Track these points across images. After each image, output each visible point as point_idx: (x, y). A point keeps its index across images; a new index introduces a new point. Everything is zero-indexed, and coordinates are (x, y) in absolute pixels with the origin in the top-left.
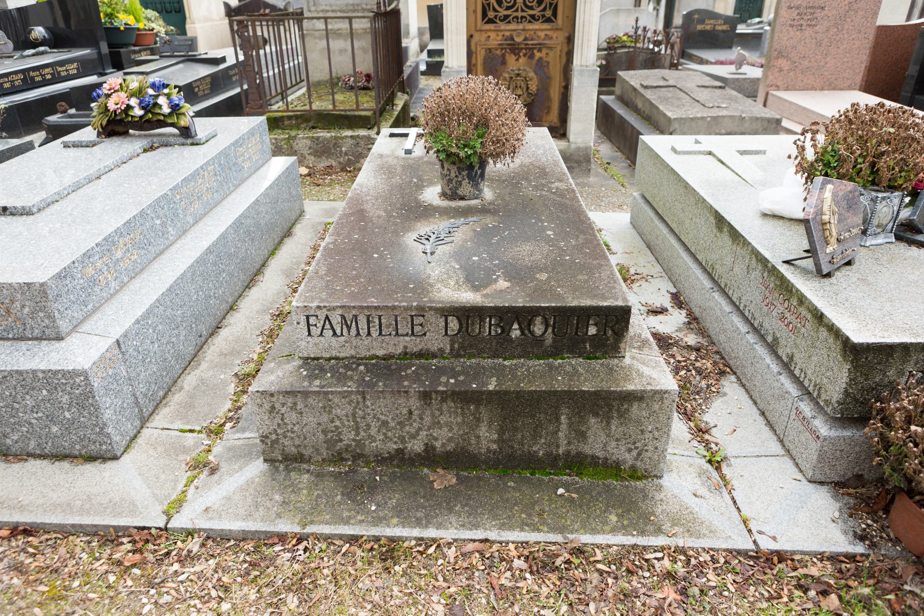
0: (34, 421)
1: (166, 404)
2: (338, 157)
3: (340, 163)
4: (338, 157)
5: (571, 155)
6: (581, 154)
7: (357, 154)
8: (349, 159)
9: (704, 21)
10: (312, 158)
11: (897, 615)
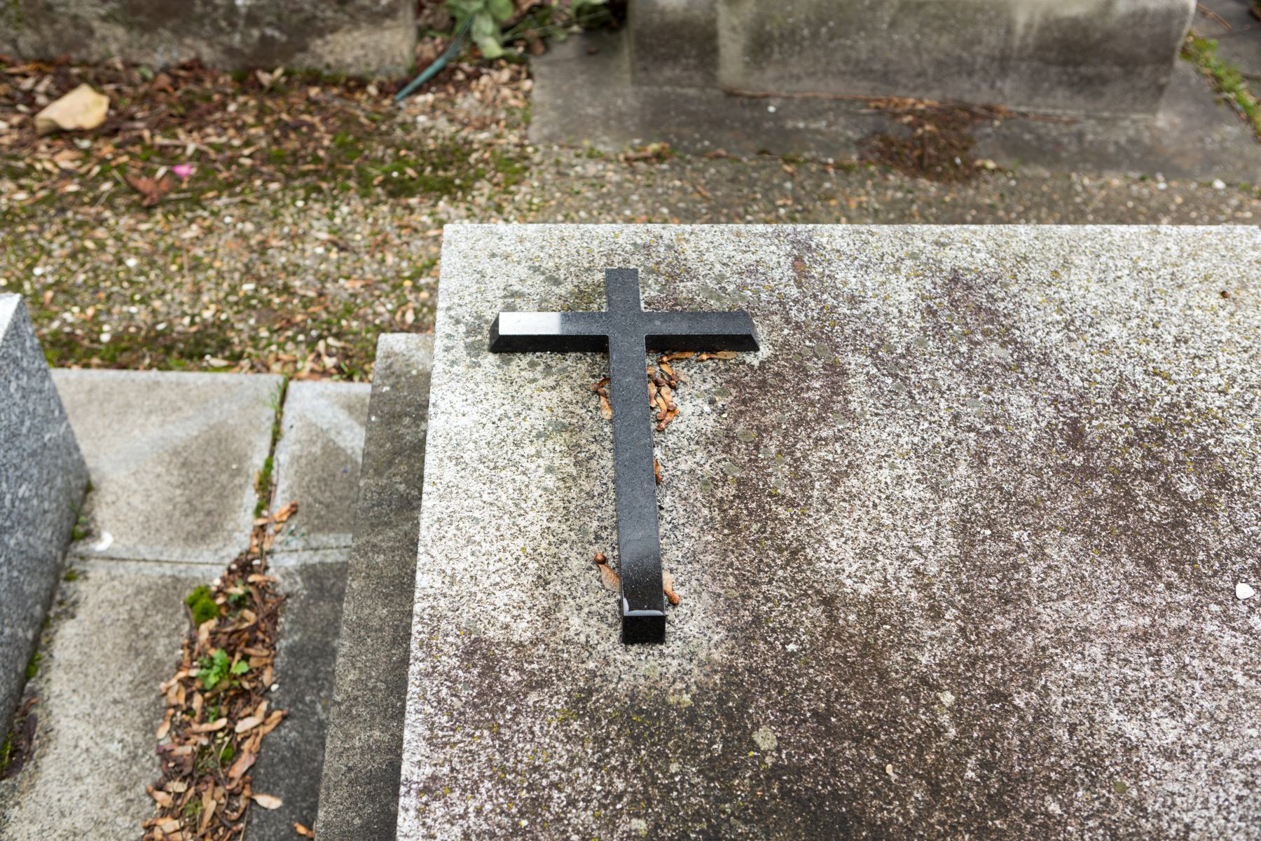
0: (430, 21)
1: (1089, 81)
2: (220, 31)
3: (230, 51)
4: (220, 31)
5: (1109, 36)
6: (1144, 33)
7: (295, 19)
8: (264, 39)
9: (202, 356)
10: (120, 32)
11: (473, 838)
